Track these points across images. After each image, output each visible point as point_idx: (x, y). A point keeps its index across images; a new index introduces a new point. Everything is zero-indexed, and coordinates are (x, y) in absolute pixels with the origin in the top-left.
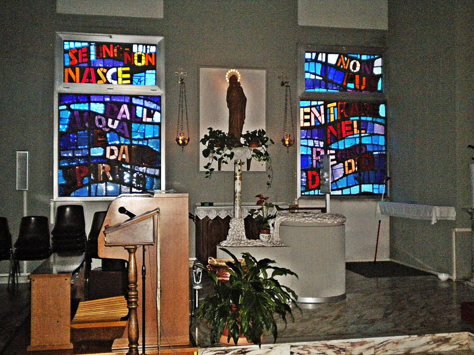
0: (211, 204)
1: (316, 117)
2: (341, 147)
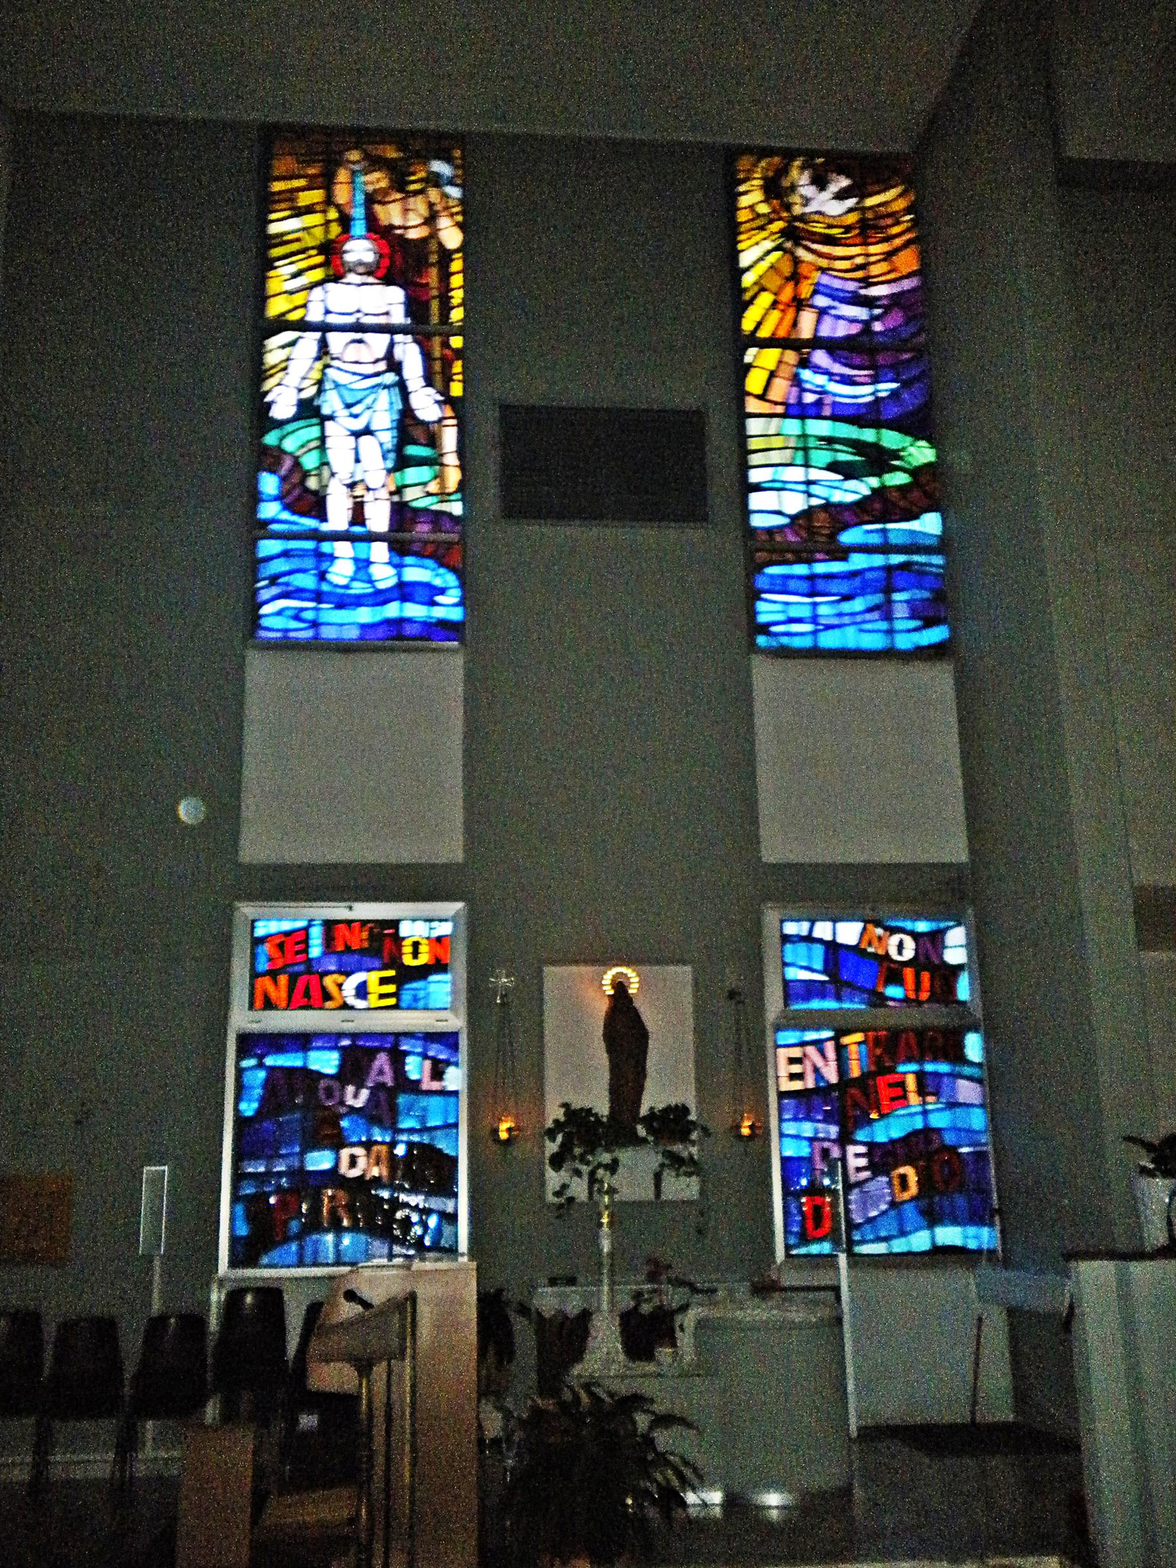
0: (572, 1281)
1: (816, 1070)
2: (881, 1138)
